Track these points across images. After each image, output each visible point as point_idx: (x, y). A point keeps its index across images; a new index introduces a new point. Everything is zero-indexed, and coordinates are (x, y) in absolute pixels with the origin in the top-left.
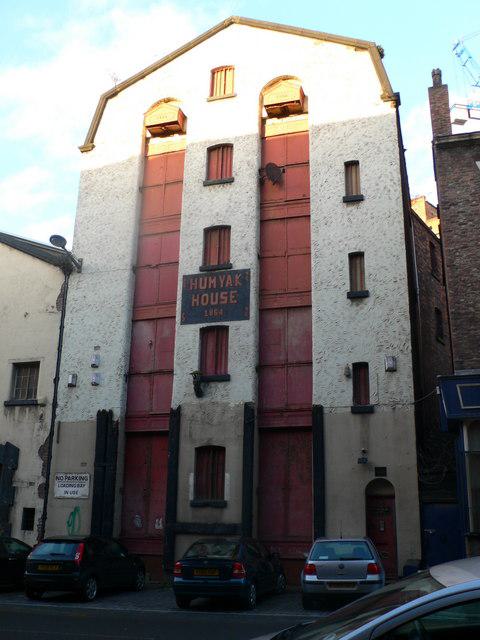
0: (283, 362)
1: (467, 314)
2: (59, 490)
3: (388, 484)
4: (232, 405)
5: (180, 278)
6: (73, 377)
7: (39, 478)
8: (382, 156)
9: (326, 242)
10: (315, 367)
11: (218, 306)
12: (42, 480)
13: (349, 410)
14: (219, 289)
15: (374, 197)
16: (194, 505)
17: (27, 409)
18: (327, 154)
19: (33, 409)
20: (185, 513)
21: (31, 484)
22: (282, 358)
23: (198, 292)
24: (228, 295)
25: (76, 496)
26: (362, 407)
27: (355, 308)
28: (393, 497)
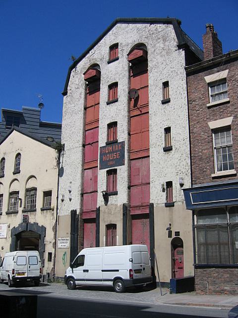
0: (139, 184)
4: (119, 205)
12: (54, 241)
14: (113, 152)
21: (50, 242)
26: (170, 205)
27: (167, 155)
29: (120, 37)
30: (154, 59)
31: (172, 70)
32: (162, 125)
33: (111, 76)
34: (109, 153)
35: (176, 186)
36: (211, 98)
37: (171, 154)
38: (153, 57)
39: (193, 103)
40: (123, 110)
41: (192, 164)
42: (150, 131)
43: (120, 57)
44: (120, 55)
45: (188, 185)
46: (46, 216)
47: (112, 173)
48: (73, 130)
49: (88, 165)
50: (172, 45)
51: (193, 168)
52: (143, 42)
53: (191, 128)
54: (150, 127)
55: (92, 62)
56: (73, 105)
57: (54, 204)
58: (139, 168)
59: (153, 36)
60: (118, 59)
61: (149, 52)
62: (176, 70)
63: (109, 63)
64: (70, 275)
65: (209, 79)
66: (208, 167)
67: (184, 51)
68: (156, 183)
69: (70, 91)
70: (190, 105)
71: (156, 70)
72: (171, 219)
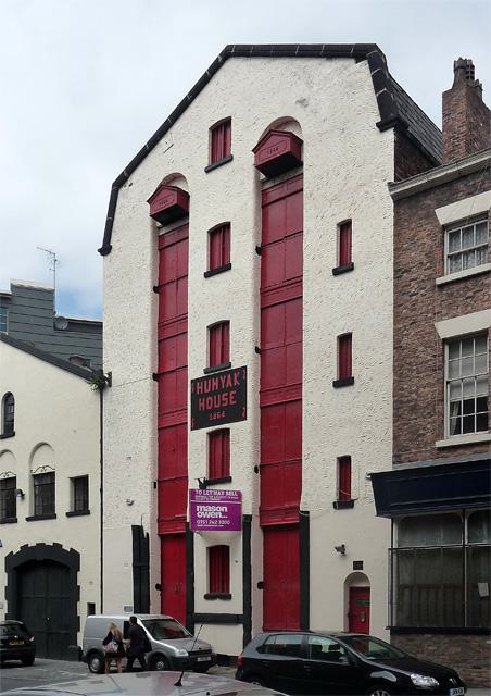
1: (409, 401)
3: (364, 578)
5: (189, 383)
11: (221, 408)
14: (221, 391)
16: (207, 597)
20: (202, 606)
36: (447, 262)
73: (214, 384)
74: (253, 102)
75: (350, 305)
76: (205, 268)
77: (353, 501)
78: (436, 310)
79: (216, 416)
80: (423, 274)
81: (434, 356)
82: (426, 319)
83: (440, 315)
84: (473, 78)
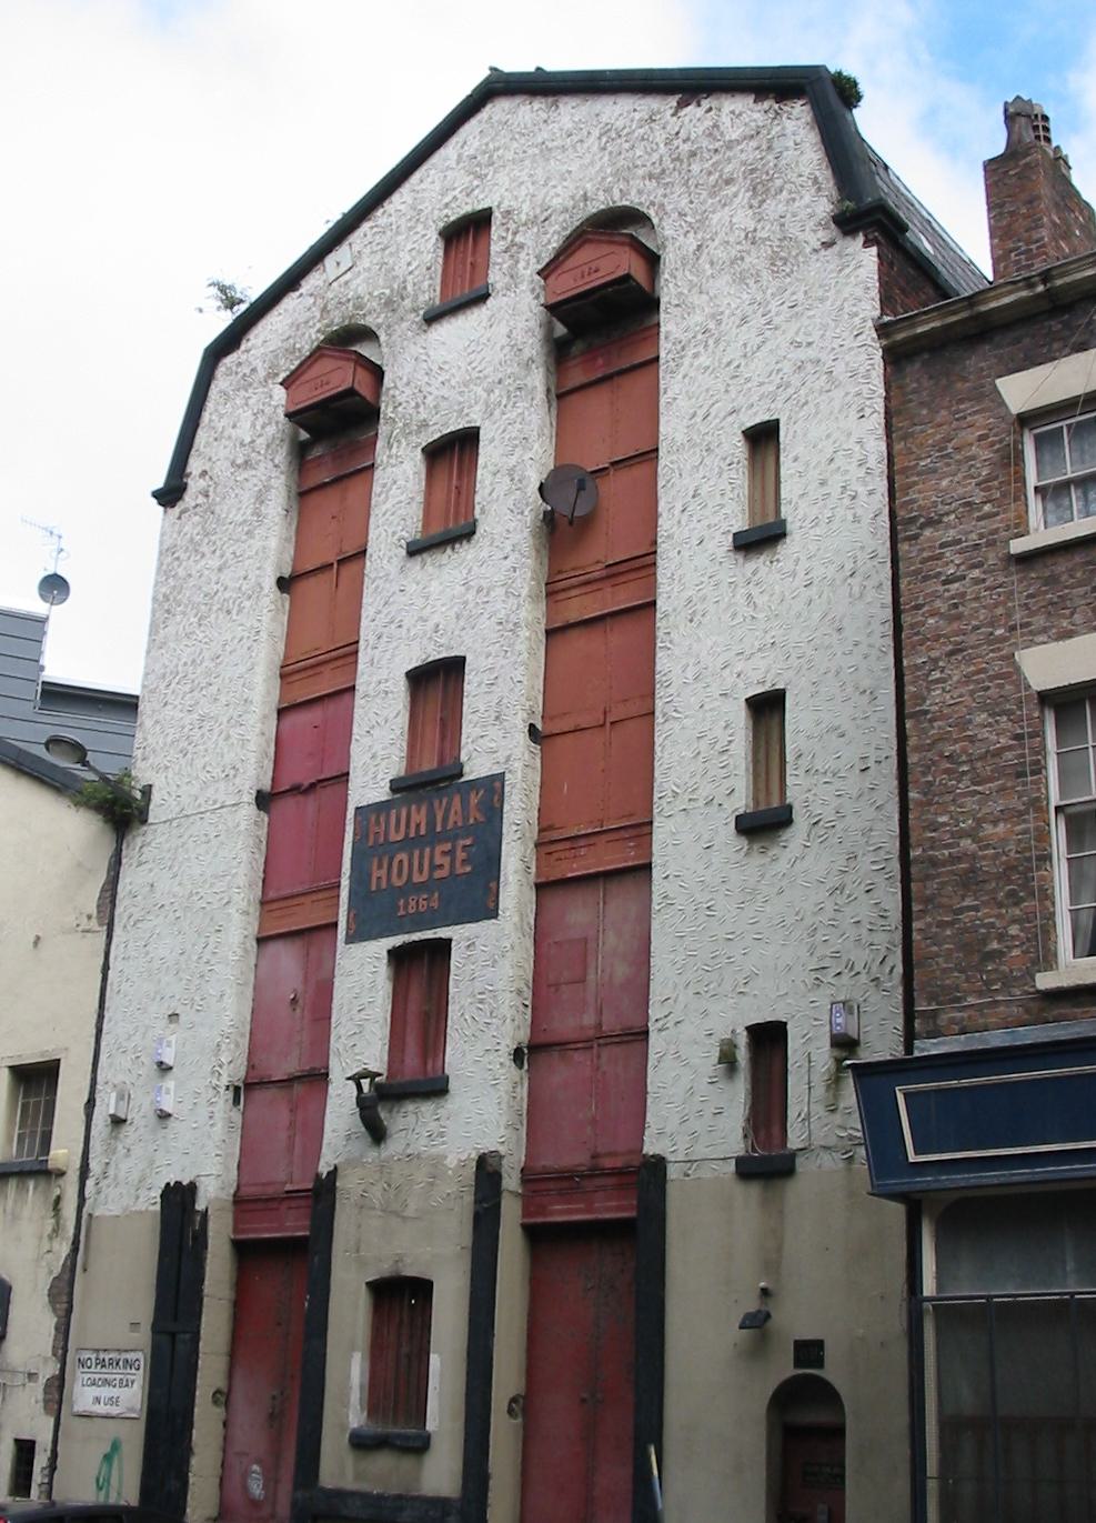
0: (586, 1039)
2: (85, 1395)
3: (826, 1394)
4: (451, 1161)
6: (120, 1097)
7: (46, 1360)
8: (838, 394)
9: (690, 674)
10: (656, 1042)
12: (52, 1369)
13: (731, 1167)
14: (432, 838)
15: (816, 522)
17: (31, 1184)
18: (701, 413)
19: (42, 1182)
21: (32, 1376)
22: (589, 1019)
23: (386, 849)
24: (451, 853)
25: (114, 1411)
26: (767, 1165)
27: (757, 860)
28: (838, 1432)
29: (503, 178)
30: (696, 299)
31: (802, 354)
32: (731, 680)
33: (445, 392)
34: (408, 843)
35: (808, 1056)
36: (1034, 505)
37: (782, 866)
38: (692, 286)
39: (927, 532)
40: (500, 591)
41: (916, 907)
42: (659, 719)
43: (498, 286)
44: (496, 277)
45: (882, 1044)
46: (15, 1217)
47: (422, 971)
48: (205, 707)
49: (292, 922)
50: (803, 215)
51: (916, 936)
52: (631, 200)
53: (910, 689)
54: (660, 692)
55: (337, 320)
56: (215, 563)
57: (64, 1151)
58: (586, 940)
59: (695, 168)
60: (482, 298)
61: (669, 259)
62: (827, 358)
63: (432, 318)
64: (347, 1436)
65: (1022, 390)
66: (1014, 930)
67: (874, 250)
68: (687, 1029)
69: (202, 483)
70: (903, 547)
71: (704, 360)
72: (772, 1262)
73: (415, 818)
74: (542, 180)
75: (765, 621)
76: (412, 528)
77: (793, 1156)
78: (1018, 617)
79: (411, 905)
80: (973, 531)
81: (1018, 737)
82: (991, 640)
83: (1031, 636)
84: (1048, 140)
